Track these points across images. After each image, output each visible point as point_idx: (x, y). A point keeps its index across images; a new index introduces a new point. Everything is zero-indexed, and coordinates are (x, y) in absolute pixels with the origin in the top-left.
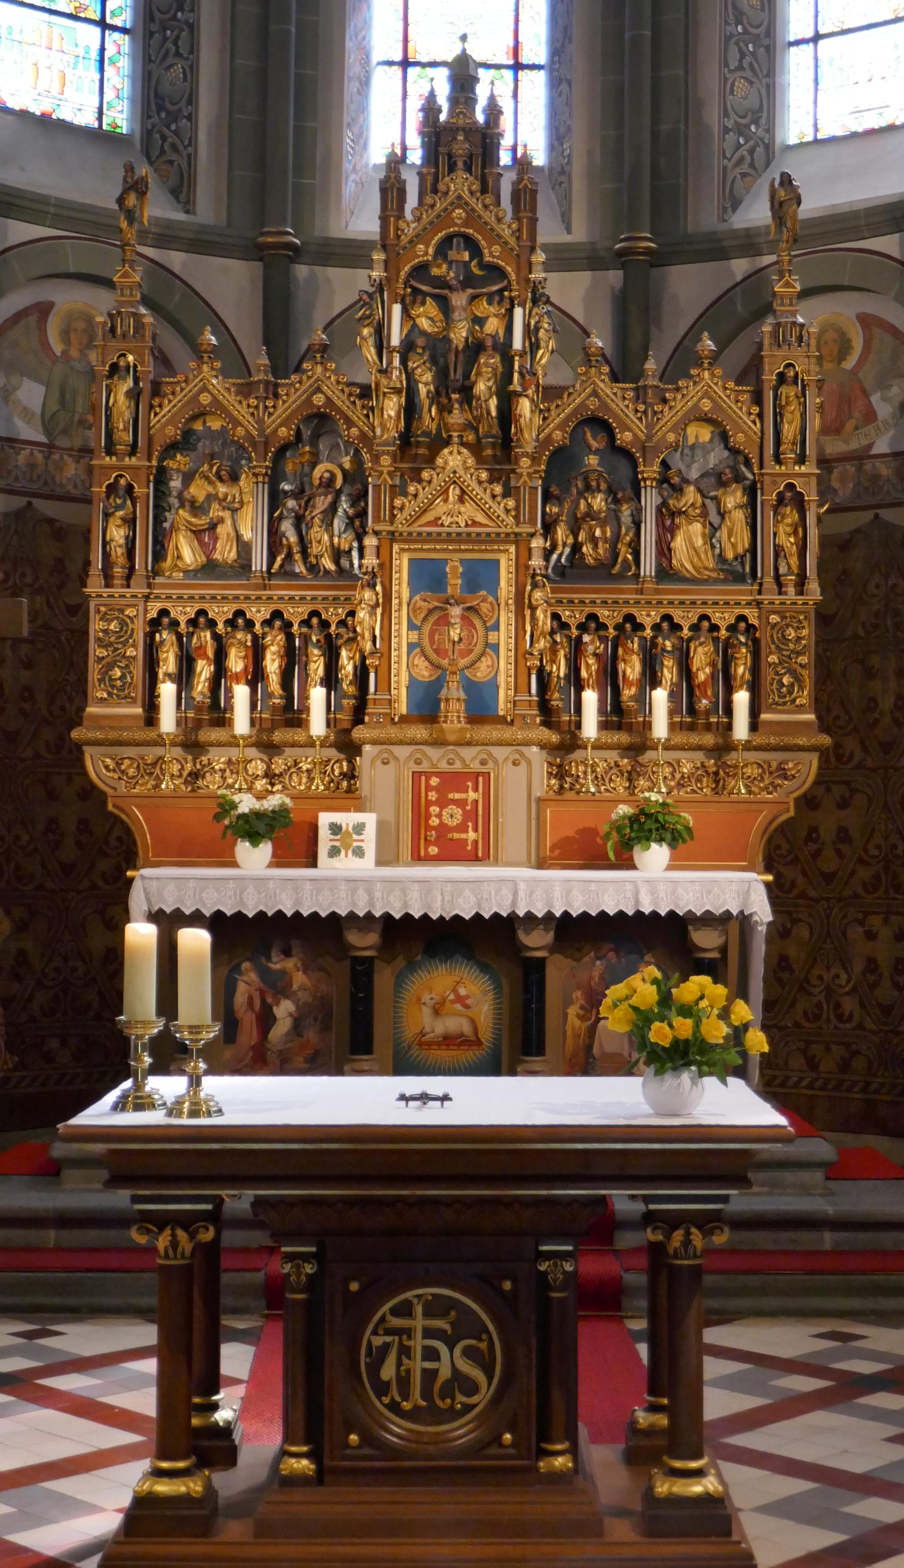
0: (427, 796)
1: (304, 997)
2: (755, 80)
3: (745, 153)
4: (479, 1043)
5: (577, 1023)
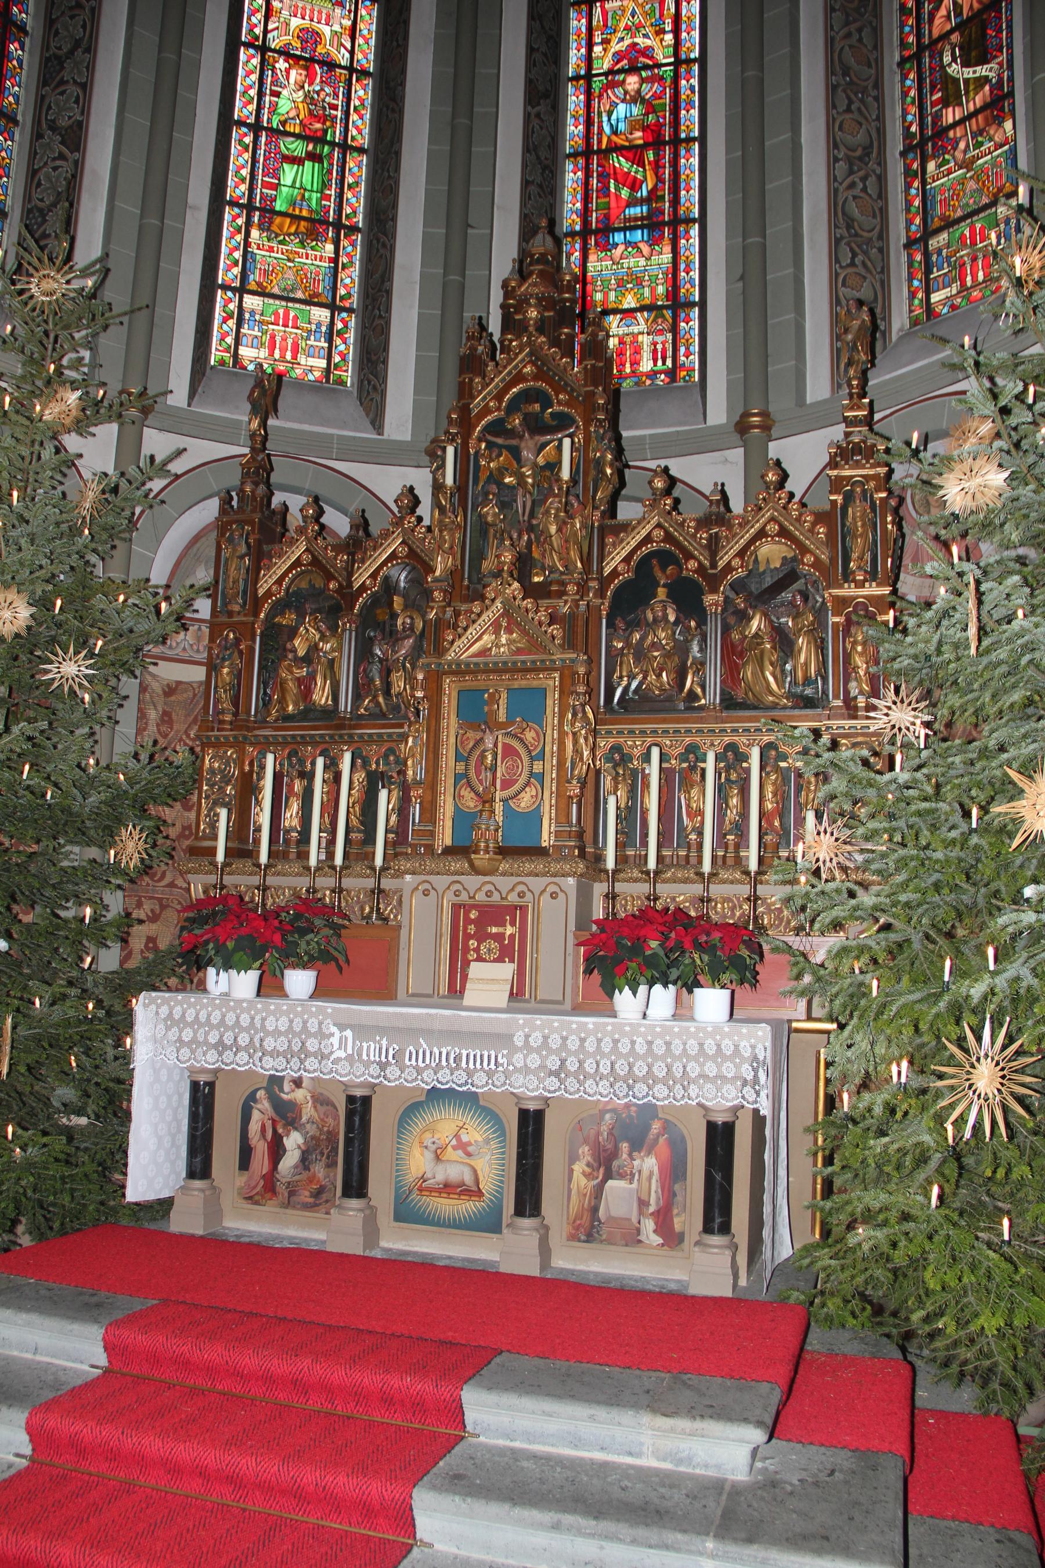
0: (465, 929)
1: (312, 1130)
2: (868, 275)
3: (857, 180)
4: (479, 1193)
5: (583, 1181)
